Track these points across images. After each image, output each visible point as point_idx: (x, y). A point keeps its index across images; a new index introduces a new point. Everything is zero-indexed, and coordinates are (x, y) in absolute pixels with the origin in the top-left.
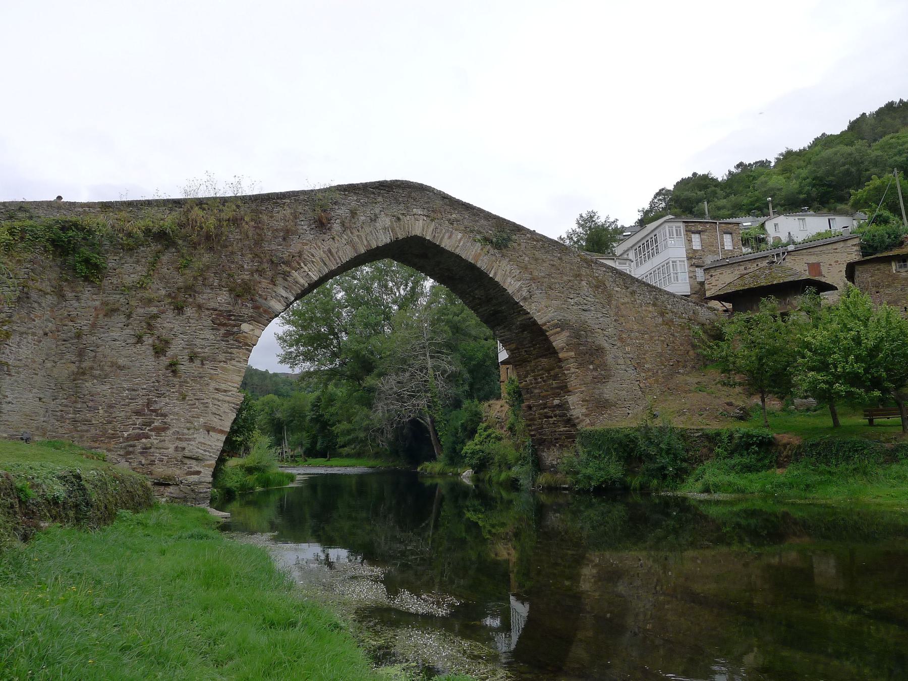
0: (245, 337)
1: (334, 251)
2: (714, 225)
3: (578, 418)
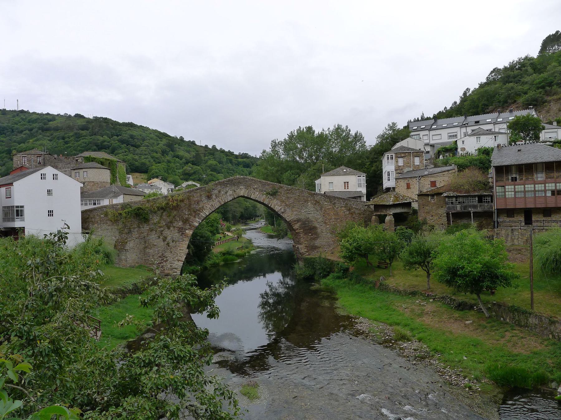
1: (213, 205)
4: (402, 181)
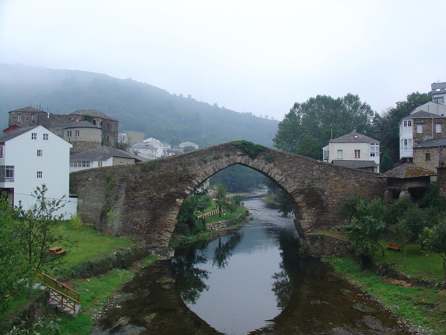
0: (178, 203)
1: (207, 172)
2: (431, 120)
3: (305, 229)
4: (421, 150)
